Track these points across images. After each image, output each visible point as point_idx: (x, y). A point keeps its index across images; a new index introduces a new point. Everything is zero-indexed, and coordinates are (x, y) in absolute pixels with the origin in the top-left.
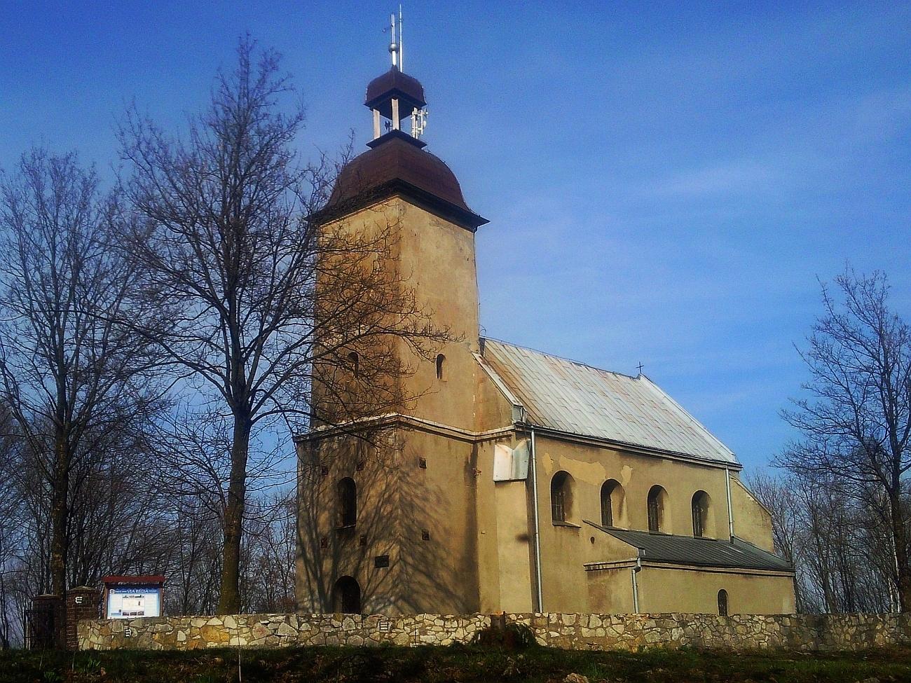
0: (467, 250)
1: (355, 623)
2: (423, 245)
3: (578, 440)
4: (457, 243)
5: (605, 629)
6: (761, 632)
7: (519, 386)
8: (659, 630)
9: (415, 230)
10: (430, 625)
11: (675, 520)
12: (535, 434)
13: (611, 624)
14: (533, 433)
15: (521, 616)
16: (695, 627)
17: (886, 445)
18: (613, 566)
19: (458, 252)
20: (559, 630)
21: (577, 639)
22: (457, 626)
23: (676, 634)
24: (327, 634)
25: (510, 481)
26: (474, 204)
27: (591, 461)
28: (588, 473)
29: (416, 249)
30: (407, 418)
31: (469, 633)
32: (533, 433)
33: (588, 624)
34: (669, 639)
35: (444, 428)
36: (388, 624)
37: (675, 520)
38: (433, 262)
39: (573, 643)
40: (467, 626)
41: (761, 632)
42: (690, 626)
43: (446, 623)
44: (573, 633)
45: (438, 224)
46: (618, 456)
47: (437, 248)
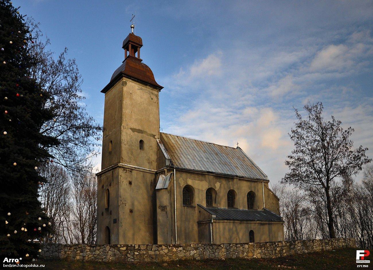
0: (155, 99)
1: (56, 247)
2: (134, 97)
3: (195, 172)
4: (150, 96)
5: (159, 251)
6: (233, 251)
7: (177, 152)
8: (184, 251)
9: (131, 92)
10: (84, 249)
11: (242, 203)
12: (175, 170)
13: (162, 249)
14: (175, 170)
15: (122, 246)
16: (201, 250)
17: (323, 169)
18: (205, 222)
19: (151, 100)
20: (139, 252)
21: (146, 255)
22: (95, 249)
23: (192, 253)
24: (45, 251)
25: (161, 189)
26: (159, 80)
27: (202, 181)
28: (200, 187)
29: (131, 99)
30: (123, 165)
31: (100, 252)
32: (175, 170)
33: (152, 249)
34: (189, 255)
35: (145, 170)
36: (68, 248)
37: (242, 203)
38: (139, 104)
39: (145, 257)
40: (99, 249)
41: (233, 251)
42: (199, 249)
43: (91, 248)
44: (145, 253)
45: (141, 89)
46: (214, 178)
47: (141, 98)
